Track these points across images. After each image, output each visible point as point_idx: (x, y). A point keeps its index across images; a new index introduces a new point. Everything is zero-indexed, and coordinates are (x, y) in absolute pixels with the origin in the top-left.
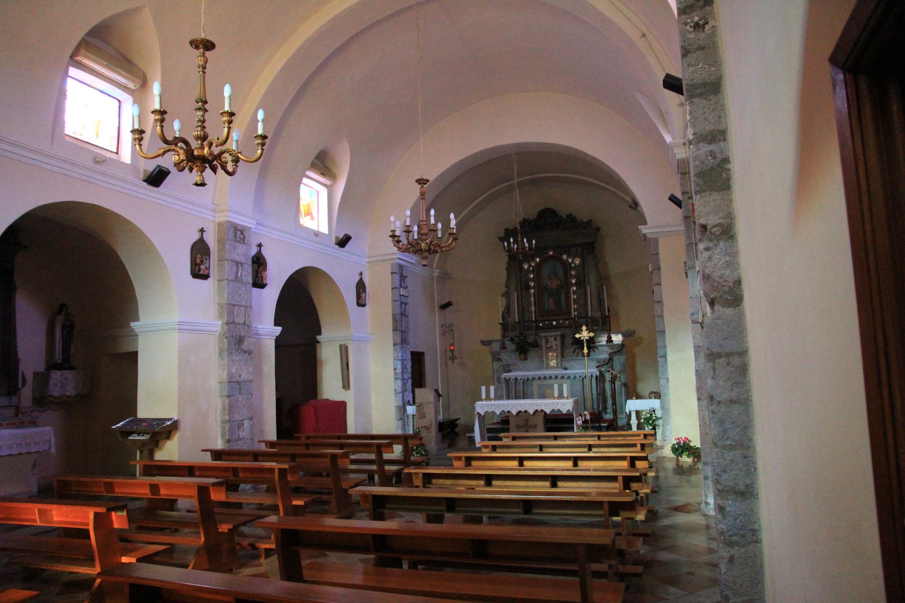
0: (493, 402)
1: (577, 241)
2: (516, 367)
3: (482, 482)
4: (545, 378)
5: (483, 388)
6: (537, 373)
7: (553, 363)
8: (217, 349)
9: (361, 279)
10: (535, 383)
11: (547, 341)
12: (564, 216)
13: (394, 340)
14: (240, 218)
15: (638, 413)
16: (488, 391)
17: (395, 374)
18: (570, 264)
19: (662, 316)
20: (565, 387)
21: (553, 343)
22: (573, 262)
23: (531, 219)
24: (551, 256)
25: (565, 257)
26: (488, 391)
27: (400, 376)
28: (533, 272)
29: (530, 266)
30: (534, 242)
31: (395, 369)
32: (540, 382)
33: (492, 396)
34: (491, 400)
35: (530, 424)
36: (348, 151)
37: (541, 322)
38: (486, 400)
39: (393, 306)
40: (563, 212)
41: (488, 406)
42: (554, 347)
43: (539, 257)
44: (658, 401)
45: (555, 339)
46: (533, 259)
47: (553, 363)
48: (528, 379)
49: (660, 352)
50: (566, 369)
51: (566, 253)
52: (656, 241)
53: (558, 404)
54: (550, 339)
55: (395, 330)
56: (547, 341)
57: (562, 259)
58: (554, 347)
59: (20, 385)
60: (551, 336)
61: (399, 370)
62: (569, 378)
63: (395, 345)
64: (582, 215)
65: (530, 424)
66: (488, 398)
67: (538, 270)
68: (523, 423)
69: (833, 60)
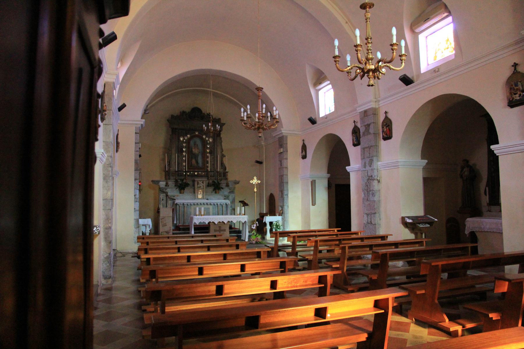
0: (203, 217)
2: (178, 197)
3: (368, 249)
4: (207, 204)
6: (191, 201)
7: (200, 196)
8: (102, 175)
9: (304, 143)
10: (193, 207)
11: (198, 184)
12: (206, 114)
13: (135, 176)
14: (366, 106)
15: (271, 223)
16: (200, 211)
17: (135, 198)
18: (207, 141)
19: (287, 175)
20: (203, 209)
21: (201, 184)
22: (209, 140)
25: (204, 137)
26: (200, 211)
27: (138, 200)
28: (186, 142)
29: (184, 139)
31: (135, 196)
32: (206, 206)
33: (203, 213)
34: (202, 215)
35: (222, 229)
36: (136, 51)
37: (188, 172)
38: (199, 215)
41: (201, 219)
42: (202, 187)
44: (280, 217)
45: (203, 183)
47: (200, 196)
49: (285, 193)
50: (207, 199)
52: (287, 137)
53: (203, 218)
54: (200, 182)
55: (136, 170)
56: (198, 184)
57: (203, 138)
59: (487, 188)
60: (200, 181)
61: (138, 196)
62: (211, 204)
63: (135, 179)
65: (222, 229)
66: (200, 214)
67: (188, 142)
68: (218, 229)
69: (405, 75)
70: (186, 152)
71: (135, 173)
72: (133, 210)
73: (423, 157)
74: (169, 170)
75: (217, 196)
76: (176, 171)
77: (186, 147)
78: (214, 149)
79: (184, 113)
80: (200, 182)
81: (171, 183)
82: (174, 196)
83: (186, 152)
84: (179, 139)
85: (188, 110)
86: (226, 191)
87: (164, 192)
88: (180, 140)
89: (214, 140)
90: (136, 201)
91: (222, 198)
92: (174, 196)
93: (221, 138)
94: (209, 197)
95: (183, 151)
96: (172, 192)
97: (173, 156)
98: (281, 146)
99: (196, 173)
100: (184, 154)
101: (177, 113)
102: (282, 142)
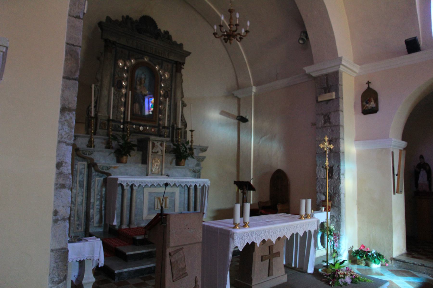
1: (171, 58)
5: (304, 201)
13: (63, 98)
17: (60, 174)
23: (134, 19)
24: (145, 63)
28: (127, 71)
29: (125, 65)
30: (248, 24)
31: (59, 165)
39: (71, 27)
40: (162, 27)
42: (160, 153)
43: (136, 59)
45: (161, 145)
46: (129, 59)
48: (143, 185)
51: (159, 64)
56: (153, 145)
58: (160, 153)
60: (158, 141)
63: (64, 110)
64: (176, 38)
67: (132, 70)
70: (126, 87)
71: (65, 88)
72: (50, 217)
73: (403, 139)
74: (96, 116)
75: (180, 169)
76: (109, 120)
77: (127, 80)
78: (171, 90)
79: (127, 19)
80: (158, 144)
81: (98, 141)
82: (108, 168)
83: (126, 87)
84: (116, 64)
85: (135, 16)
86: (190, 162)
87: (84, 158)
88: (119, 65)
89: (171, 76)
90: (63, 186)
91: (189, 173)
92: (108, 168)
93: (182, 76)
94: (169, 173)
95: (122, 87)
96: (103, 158)
97: (105, 92)
98: (327, 90)
99: (141, 128)
100: (124, 91)
101: (116, 16)
102: (330, 83)
